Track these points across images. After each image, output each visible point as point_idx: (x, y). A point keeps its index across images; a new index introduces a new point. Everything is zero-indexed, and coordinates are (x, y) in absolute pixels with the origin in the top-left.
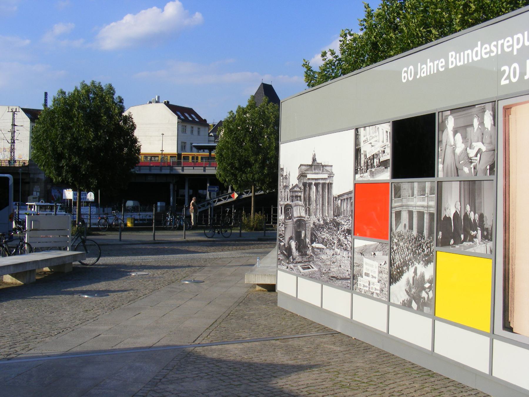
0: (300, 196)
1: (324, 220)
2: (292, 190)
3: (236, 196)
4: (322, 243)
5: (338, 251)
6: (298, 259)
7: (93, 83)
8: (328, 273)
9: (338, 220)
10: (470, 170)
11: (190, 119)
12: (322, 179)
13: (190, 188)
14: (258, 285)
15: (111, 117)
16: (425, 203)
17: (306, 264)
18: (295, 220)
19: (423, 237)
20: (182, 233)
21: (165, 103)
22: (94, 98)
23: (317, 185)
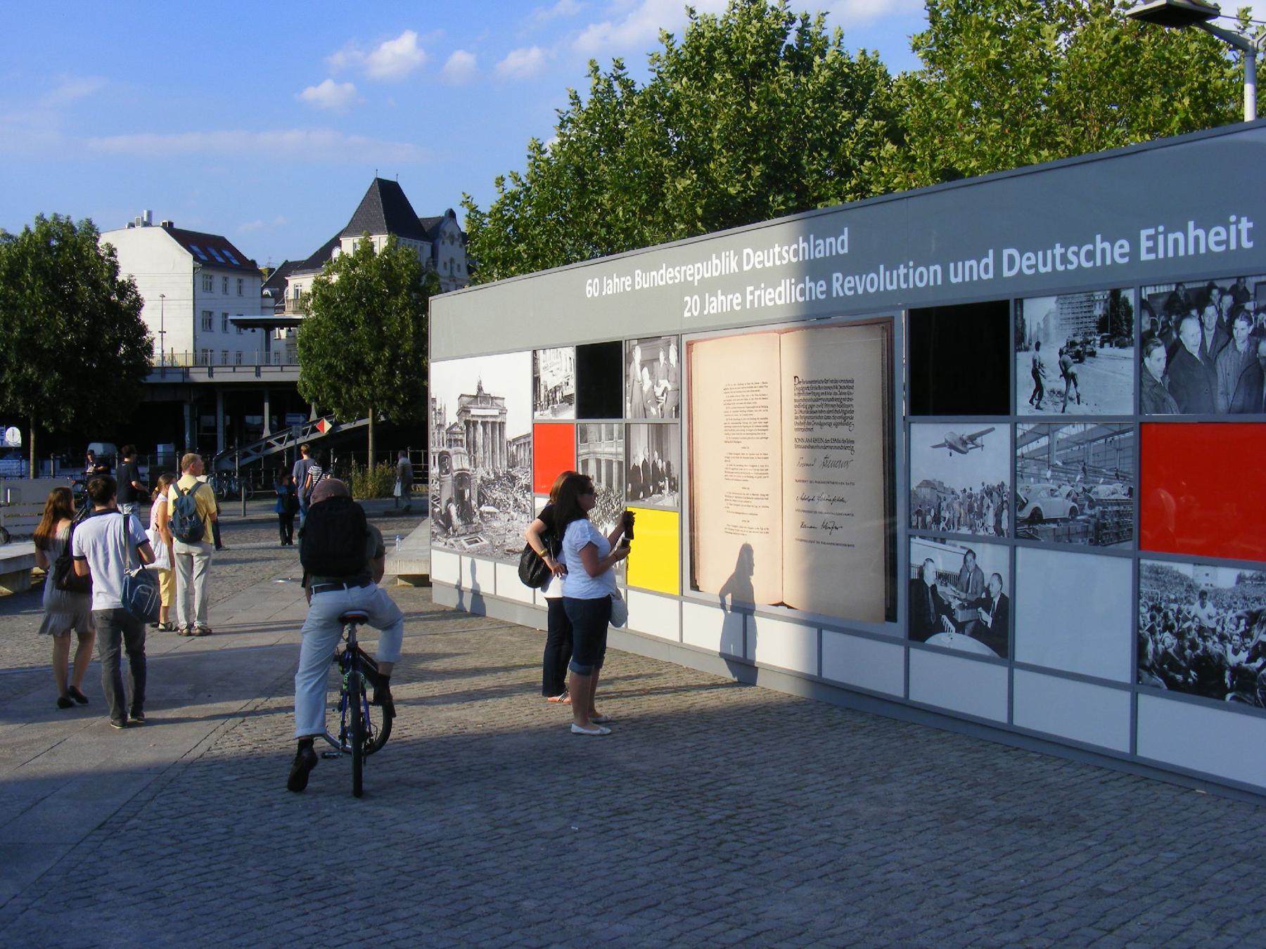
0: (461, 440)
1: (495, 473)
2: (449, 431)
3: (327, 426)
4: (493, 505)
5: (515, 515)
6: (462, 530)
7: (56, 217)
8: (502, 545)
9: (514, 472)
10: (657, 411)
11: (221, 260)
12: (491, 416)
13: (226, 413)
14: (400, 576)
15: (95, 285)
16: (613, 450)
17: (473, 536)
18: (455, 474)
19: (612, 490)
20: (239, 506)
21: (164, 226)
22: (59, 249)
23: (484, 424)
